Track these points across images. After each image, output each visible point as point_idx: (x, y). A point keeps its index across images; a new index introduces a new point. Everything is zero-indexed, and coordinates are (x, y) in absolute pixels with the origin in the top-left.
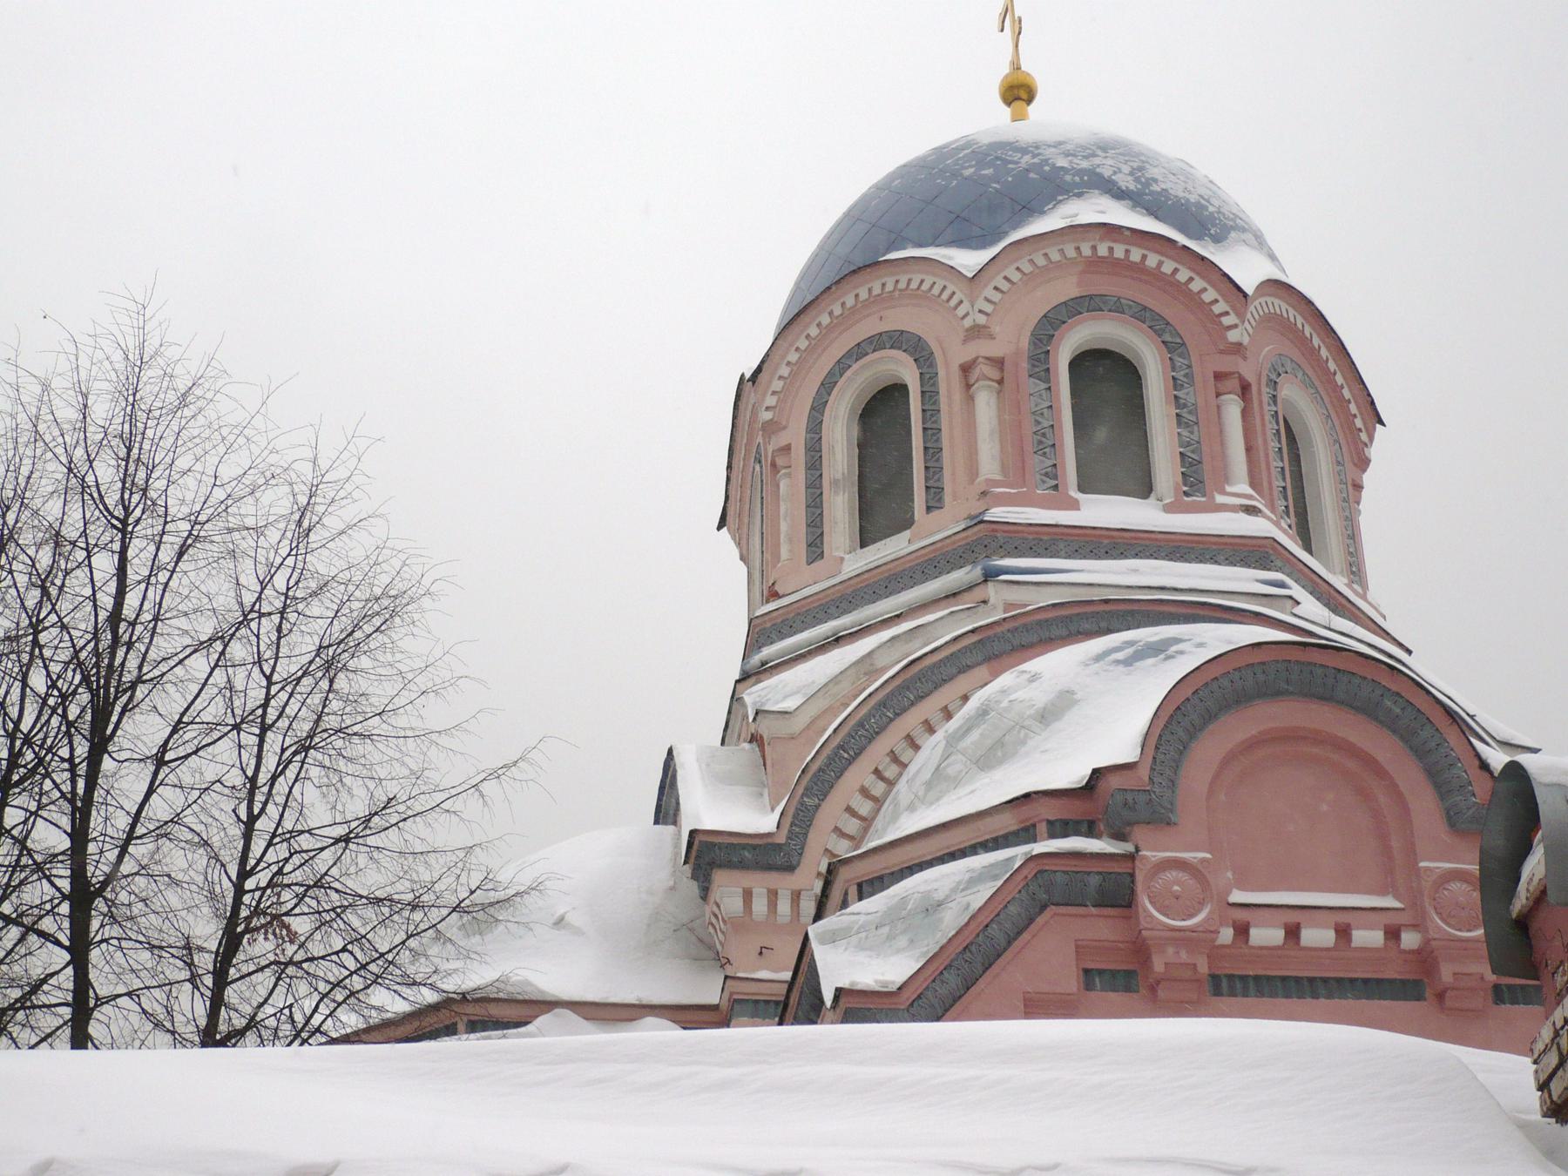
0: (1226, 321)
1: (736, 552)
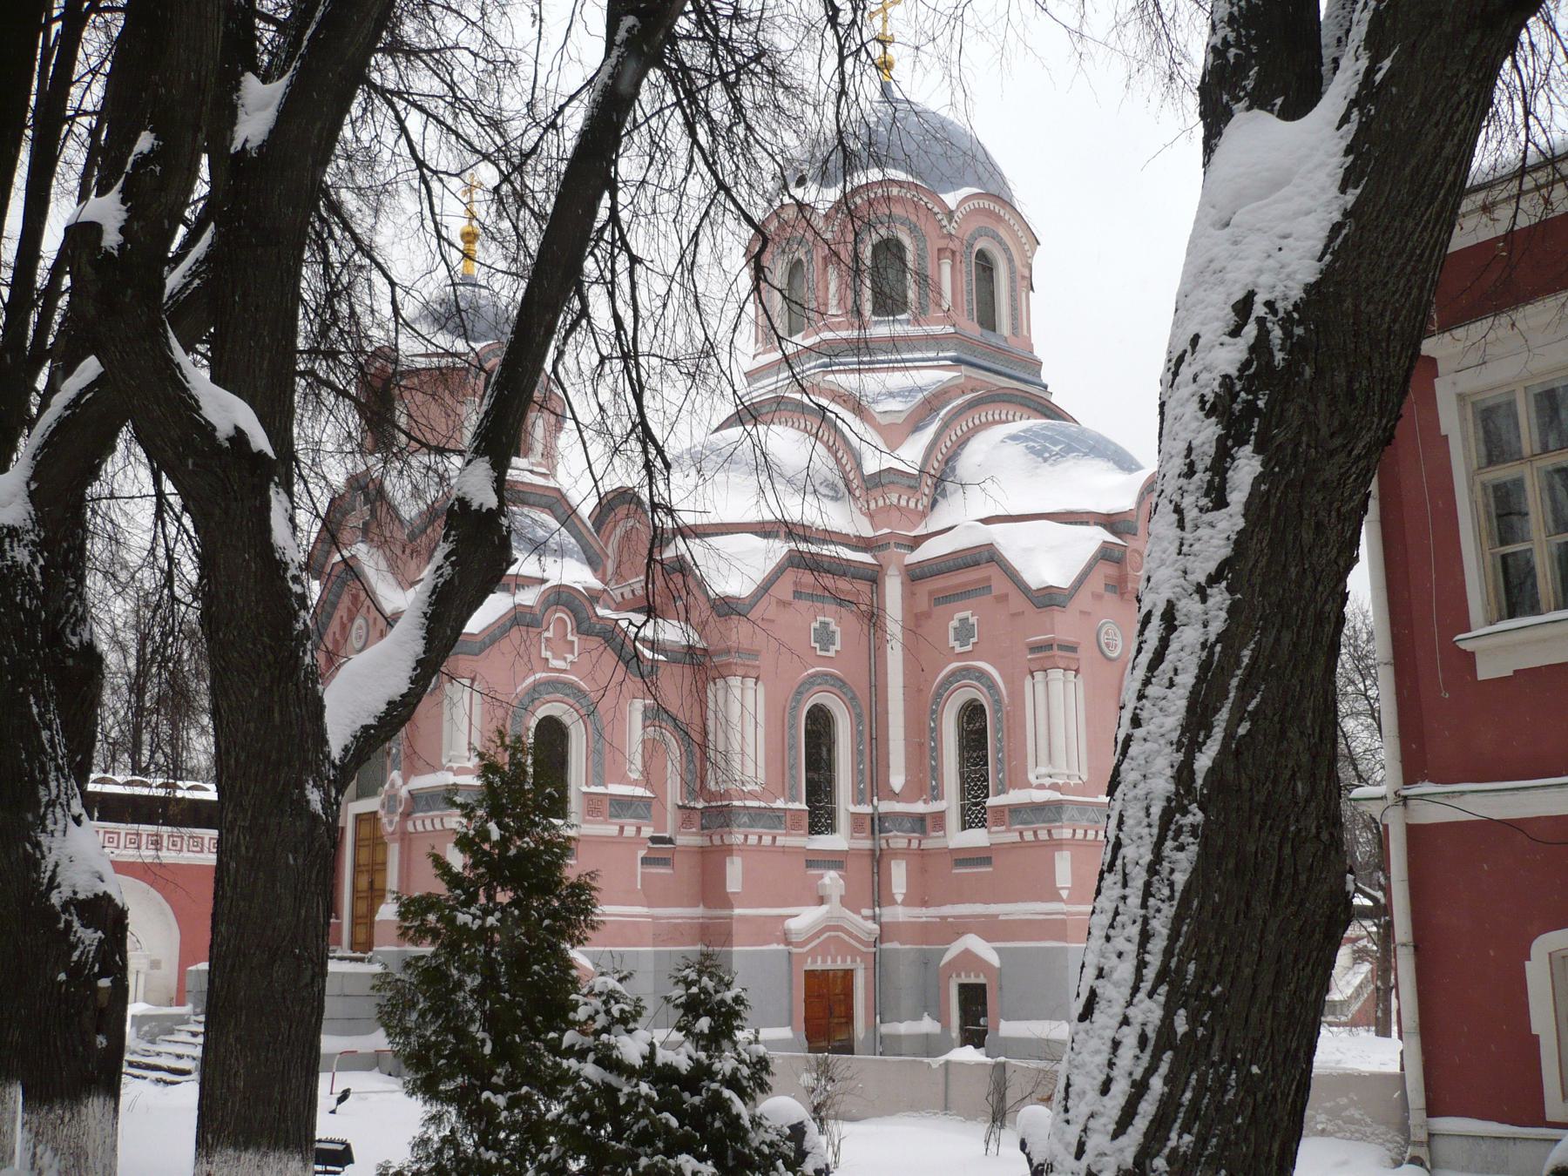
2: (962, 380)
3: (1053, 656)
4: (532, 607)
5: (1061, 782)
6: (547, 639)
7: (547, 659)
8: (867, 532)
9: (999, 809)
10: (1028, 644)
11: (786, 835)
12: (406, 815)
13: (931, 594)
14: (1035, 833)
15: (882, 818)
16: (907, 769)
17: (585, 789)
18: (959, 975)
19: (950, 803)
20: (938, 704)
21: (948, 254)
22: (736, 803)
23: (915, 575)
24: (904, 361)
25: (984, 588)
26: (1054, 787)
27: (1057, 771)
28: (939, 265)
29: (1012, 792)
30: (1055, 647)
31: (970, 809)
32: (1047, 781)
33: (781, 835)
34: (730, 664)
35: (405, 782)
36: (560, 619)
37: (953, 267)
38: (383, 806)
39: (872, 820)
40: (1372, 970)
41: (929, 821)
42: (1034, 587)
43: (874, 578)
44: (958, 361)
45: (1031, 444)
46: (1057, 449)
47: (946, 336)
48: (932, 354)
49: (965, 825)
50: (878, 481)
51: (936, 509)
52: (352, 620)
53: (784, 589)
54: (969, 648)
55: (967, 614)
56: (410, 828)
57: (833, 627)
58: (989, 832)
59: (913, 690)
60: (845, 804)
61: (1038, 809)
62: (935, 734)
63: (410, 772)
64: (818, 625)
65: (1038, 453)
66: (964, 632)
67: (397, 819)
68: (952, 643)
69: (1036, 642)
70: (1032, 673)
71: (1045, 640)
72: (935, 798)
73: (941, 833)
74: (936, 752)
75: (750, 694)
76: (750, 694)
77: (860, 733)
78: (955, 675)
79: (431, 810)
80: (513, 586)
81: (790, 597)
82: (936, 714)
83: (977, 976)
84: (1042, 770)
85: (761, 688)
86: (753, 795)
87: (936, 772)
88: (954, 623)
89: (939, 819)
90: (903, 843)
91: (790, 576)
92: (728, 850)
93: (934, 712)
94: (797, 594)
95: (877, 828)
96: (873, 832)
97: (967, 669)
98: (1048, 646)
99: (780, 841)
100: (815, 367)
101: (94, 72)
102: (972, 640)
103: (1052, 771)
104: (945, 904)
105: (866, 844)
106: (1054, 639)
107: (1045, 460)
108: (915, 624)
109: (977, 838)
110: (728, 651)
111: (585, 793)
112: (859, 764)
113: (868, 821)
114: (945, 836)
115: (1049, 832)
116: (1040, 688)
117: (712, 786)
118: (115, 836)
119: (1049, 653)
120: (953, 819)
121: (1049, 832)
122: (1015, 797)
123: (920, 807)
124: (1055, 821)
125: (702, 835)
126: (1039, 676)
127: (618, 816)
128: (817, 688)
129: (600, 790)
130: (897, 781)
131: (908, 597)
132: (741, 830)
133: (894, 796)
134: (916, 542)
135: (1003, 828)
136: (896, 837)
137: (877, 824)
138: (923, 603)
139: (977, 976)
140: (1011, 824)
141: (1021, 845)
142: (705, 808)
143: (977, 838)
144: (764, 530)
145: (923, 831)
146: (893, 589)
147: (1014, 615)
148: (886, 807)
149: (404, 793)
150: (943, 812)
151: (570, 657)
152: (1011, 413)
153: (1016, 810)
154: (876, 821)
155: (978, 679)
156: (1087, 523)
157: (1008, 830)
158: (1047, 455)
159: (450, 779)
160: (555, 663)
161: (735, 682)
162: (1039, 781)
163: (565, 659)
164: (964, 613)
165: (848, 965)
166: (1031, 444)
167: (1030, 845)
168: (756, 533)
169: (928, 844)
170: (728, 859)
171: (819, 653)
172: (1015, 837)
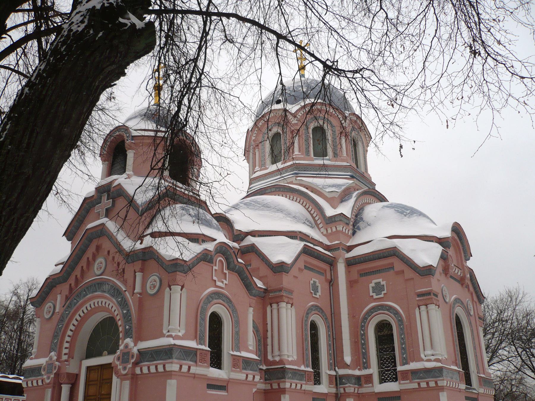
2: (354, 185)
3: (432, 298)
4: (210, 251)
5: (440, 358)
6: (215, 270)
7: (215, 281)
8: (327, 242)
9: (403, 372)
10: (416, 293)
11: (306, 384)
12: (136, 364)
13: (358, 271)
14: (428, 383)
15: (342, 377)
16: (352, 354)
17: (232, 353)
19: (374, 370)
20: (365, 323)
22: (287, 366)
23: (350, 263)
24: (329, 175)
25: (391, 267)
26: (437, 360)
27: (437, 352)
29: (411, 364)
30: (432, 294)
31: (384, 373)
32: (433, 358)
33: (304, 384)
34: (283, 296)
35: (135, 345)
36: (220, 261)
38: (118, 359)
39: (336, 378)
41: (363, 380)
42: (421, 266)
43: (332, 263)
44: (352, 177)
45: (397, 209)
46: (408, 212)
47: (345, 167)
49: (382, 381)
50: (332, 220)
51: (356, 235)
52: (94, 259)
53: (301, 264)
54: (382, 296)
55: (380, 280)
56: (138, 371)
57: (318, 284)
58: (400, 383)
59: (352, 316)
60: (325, 370)
61: (427, 371)
62: (364, 336)
63: (138, 339)
64: (313, 282)
65: (402, 213)
66: (378, 288)
67: (130, 366)
68: (371, 294)
69: (420, 292)
70: (419, 307)
71: (425, 291)
72: (366, 368)
73: (371, 385)
74: (365, 345)
75: (289, 311)
76: (289, 311)
77: (329, 336)
78: (374, 309)
79: (155, 360)
80: (200, 240)
81: (303, 267)
82: (364, 328)
84: (429, 352)
86: (291, 363)
87: (366, 355)
88: (372, 285)
89: (369, 378)
90: (352, 390)
91: (304, 257)
92: (283, 391)
93: (362, 326)
95: (338, 382)
96: (336, 385)
97: (382, 306)
98: (428, 293)
99: (304, 387)
100: (293, 174)
102: (383, 292)
103: (434, 353)
105: (334, 390)
106: (432, 290)
107: (405, 216)
108: (351, 284)
109: (391, 387)
110: (280, 290)
111: (232, 355)
112: (401, 335)
113: (334, 378)
114: (373, 386)
115: (436, 383)
116: (424, 314)
117: (270, 357)
119: (429, 297)
120: (376, 378)
121: (436, 383)
122: (413, 366)
123: (357, 373)
124: (439, 377)
125: (265, 384)
126: (423, 308)
127: (245, 369)
129: (238, 354)
130: (348, 359)
131: (348, 273)
132: (289, 380)
133: (346, 366)
134: (350, 249)
135: (408, 381)
136: (350, 387)
137: (337, 381)
138: (355, 275)
140: (412, 380)
141: (420, 388)
142: (267, 369)
143: (391, 387)
144: (292, 235)
145: (360, 385)
146: (341, 268)
147: (407, 280)
148: (342, 372)
149: (135, 350)
150: (372, 374)
151: (225, 282)
152: (374, 200)
153: (415, 373)
154: (338, 379)
155: (388, 310)
156: (432, 241)
157: (411, 382)
158: (405, 214)
159: (172, 341)
160: (219, 284)
161: (283, 305)
162: (427, 358)
163: (223, 282)
166: (397, 209)
167: (433, 389)
168: (288, 237)
169: (363, 390)
170: (282, 396)
171: (314, 295)
172: (415, 386)
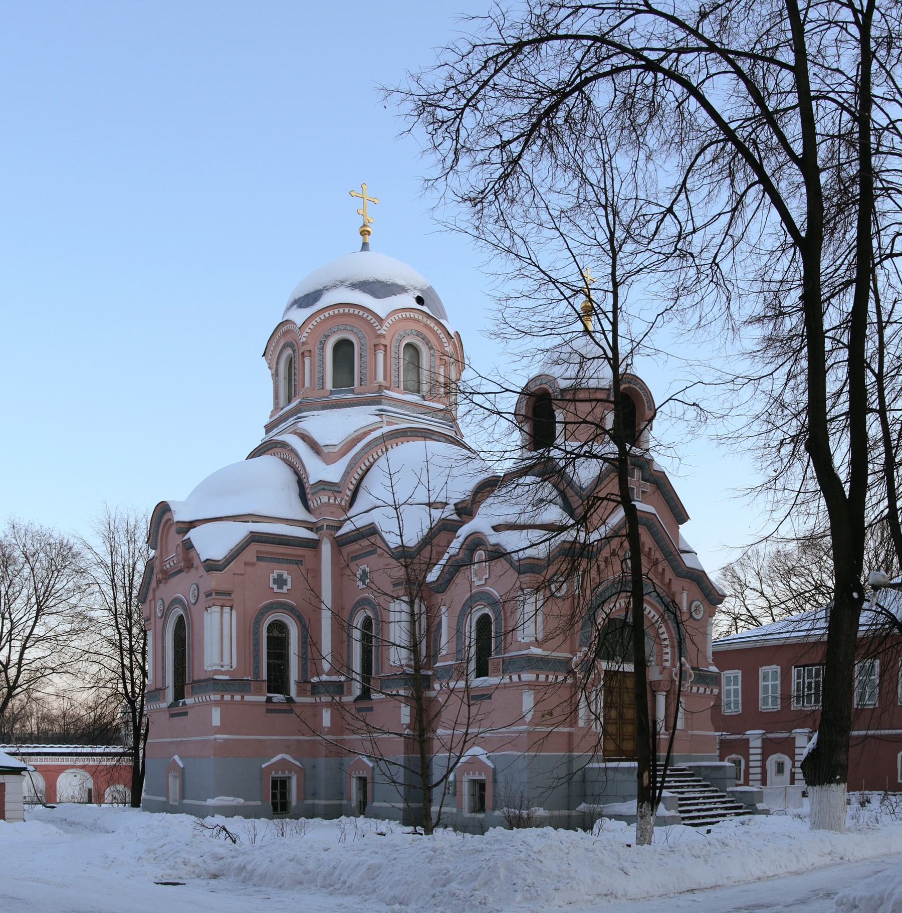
0: (445, 345)
1: (266, 365)
18: (468, 774)
21: (382, 347)
28: (375, 354)
37: (385, 355)
40: (80, 718)
48: (430, 418)
81: (255, 560)
83: (480, 774)
85: (234, 613)
94: (259, 559)
101: (839, 393)
104: (785, 754)
118: (742, 782)
128: (267, 615)
130: (326, 666)
139: (480, 774)
146: (326, 549)
164: (364, 566)
165: (287, 774)
